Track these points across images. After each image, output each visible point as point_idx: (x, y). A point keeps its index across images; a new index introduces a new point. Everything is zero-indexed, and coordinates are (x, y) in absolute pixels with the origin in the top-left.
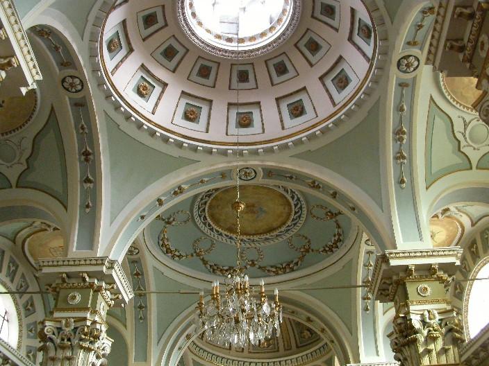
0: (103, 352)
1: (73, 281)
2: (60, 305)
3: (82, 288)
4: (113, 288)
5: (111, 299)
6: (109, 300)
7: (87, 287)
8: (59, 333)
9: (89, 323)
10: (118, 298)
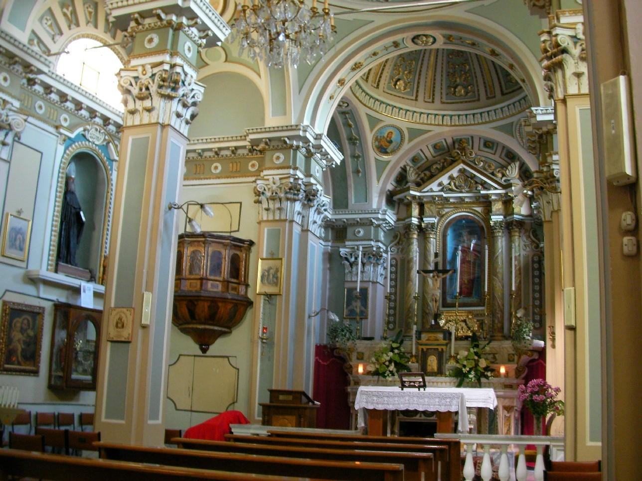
0: (193, 100)
1: (147, 21)
2: (268, 164)
3: (160, 28)
4: (327, 158)
5: (200, 38)
6: (197, 38)
7: (165, 27)
8: (136, 83)
9: (375, 249)
10: (207, 35)
